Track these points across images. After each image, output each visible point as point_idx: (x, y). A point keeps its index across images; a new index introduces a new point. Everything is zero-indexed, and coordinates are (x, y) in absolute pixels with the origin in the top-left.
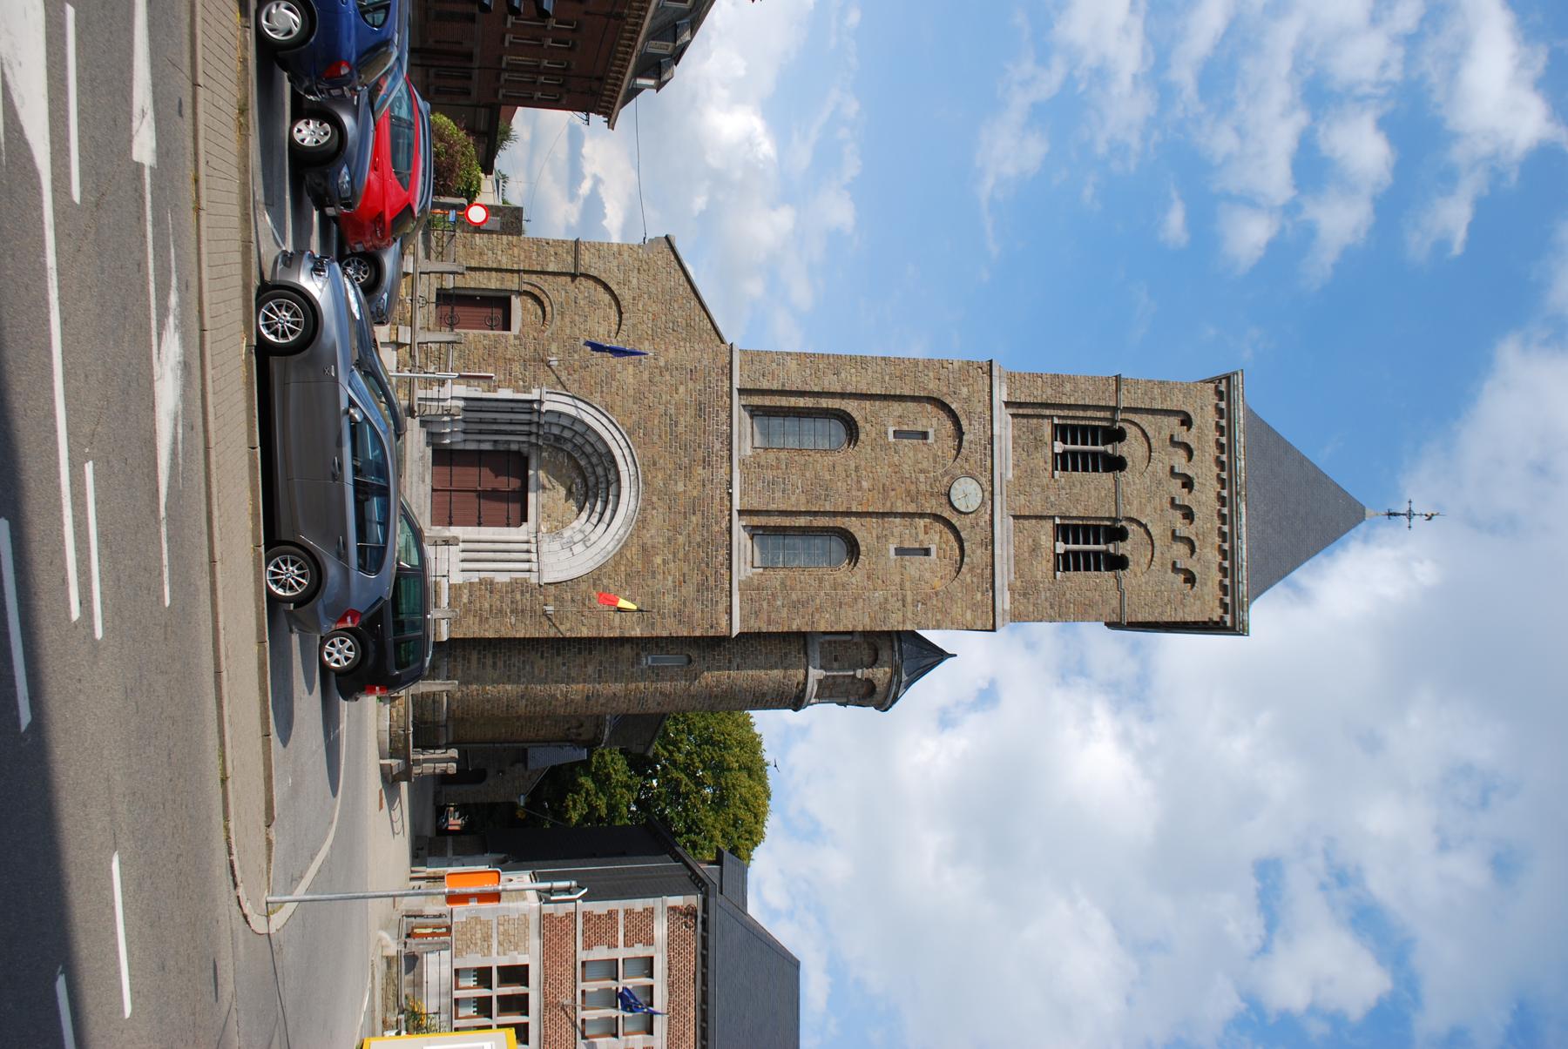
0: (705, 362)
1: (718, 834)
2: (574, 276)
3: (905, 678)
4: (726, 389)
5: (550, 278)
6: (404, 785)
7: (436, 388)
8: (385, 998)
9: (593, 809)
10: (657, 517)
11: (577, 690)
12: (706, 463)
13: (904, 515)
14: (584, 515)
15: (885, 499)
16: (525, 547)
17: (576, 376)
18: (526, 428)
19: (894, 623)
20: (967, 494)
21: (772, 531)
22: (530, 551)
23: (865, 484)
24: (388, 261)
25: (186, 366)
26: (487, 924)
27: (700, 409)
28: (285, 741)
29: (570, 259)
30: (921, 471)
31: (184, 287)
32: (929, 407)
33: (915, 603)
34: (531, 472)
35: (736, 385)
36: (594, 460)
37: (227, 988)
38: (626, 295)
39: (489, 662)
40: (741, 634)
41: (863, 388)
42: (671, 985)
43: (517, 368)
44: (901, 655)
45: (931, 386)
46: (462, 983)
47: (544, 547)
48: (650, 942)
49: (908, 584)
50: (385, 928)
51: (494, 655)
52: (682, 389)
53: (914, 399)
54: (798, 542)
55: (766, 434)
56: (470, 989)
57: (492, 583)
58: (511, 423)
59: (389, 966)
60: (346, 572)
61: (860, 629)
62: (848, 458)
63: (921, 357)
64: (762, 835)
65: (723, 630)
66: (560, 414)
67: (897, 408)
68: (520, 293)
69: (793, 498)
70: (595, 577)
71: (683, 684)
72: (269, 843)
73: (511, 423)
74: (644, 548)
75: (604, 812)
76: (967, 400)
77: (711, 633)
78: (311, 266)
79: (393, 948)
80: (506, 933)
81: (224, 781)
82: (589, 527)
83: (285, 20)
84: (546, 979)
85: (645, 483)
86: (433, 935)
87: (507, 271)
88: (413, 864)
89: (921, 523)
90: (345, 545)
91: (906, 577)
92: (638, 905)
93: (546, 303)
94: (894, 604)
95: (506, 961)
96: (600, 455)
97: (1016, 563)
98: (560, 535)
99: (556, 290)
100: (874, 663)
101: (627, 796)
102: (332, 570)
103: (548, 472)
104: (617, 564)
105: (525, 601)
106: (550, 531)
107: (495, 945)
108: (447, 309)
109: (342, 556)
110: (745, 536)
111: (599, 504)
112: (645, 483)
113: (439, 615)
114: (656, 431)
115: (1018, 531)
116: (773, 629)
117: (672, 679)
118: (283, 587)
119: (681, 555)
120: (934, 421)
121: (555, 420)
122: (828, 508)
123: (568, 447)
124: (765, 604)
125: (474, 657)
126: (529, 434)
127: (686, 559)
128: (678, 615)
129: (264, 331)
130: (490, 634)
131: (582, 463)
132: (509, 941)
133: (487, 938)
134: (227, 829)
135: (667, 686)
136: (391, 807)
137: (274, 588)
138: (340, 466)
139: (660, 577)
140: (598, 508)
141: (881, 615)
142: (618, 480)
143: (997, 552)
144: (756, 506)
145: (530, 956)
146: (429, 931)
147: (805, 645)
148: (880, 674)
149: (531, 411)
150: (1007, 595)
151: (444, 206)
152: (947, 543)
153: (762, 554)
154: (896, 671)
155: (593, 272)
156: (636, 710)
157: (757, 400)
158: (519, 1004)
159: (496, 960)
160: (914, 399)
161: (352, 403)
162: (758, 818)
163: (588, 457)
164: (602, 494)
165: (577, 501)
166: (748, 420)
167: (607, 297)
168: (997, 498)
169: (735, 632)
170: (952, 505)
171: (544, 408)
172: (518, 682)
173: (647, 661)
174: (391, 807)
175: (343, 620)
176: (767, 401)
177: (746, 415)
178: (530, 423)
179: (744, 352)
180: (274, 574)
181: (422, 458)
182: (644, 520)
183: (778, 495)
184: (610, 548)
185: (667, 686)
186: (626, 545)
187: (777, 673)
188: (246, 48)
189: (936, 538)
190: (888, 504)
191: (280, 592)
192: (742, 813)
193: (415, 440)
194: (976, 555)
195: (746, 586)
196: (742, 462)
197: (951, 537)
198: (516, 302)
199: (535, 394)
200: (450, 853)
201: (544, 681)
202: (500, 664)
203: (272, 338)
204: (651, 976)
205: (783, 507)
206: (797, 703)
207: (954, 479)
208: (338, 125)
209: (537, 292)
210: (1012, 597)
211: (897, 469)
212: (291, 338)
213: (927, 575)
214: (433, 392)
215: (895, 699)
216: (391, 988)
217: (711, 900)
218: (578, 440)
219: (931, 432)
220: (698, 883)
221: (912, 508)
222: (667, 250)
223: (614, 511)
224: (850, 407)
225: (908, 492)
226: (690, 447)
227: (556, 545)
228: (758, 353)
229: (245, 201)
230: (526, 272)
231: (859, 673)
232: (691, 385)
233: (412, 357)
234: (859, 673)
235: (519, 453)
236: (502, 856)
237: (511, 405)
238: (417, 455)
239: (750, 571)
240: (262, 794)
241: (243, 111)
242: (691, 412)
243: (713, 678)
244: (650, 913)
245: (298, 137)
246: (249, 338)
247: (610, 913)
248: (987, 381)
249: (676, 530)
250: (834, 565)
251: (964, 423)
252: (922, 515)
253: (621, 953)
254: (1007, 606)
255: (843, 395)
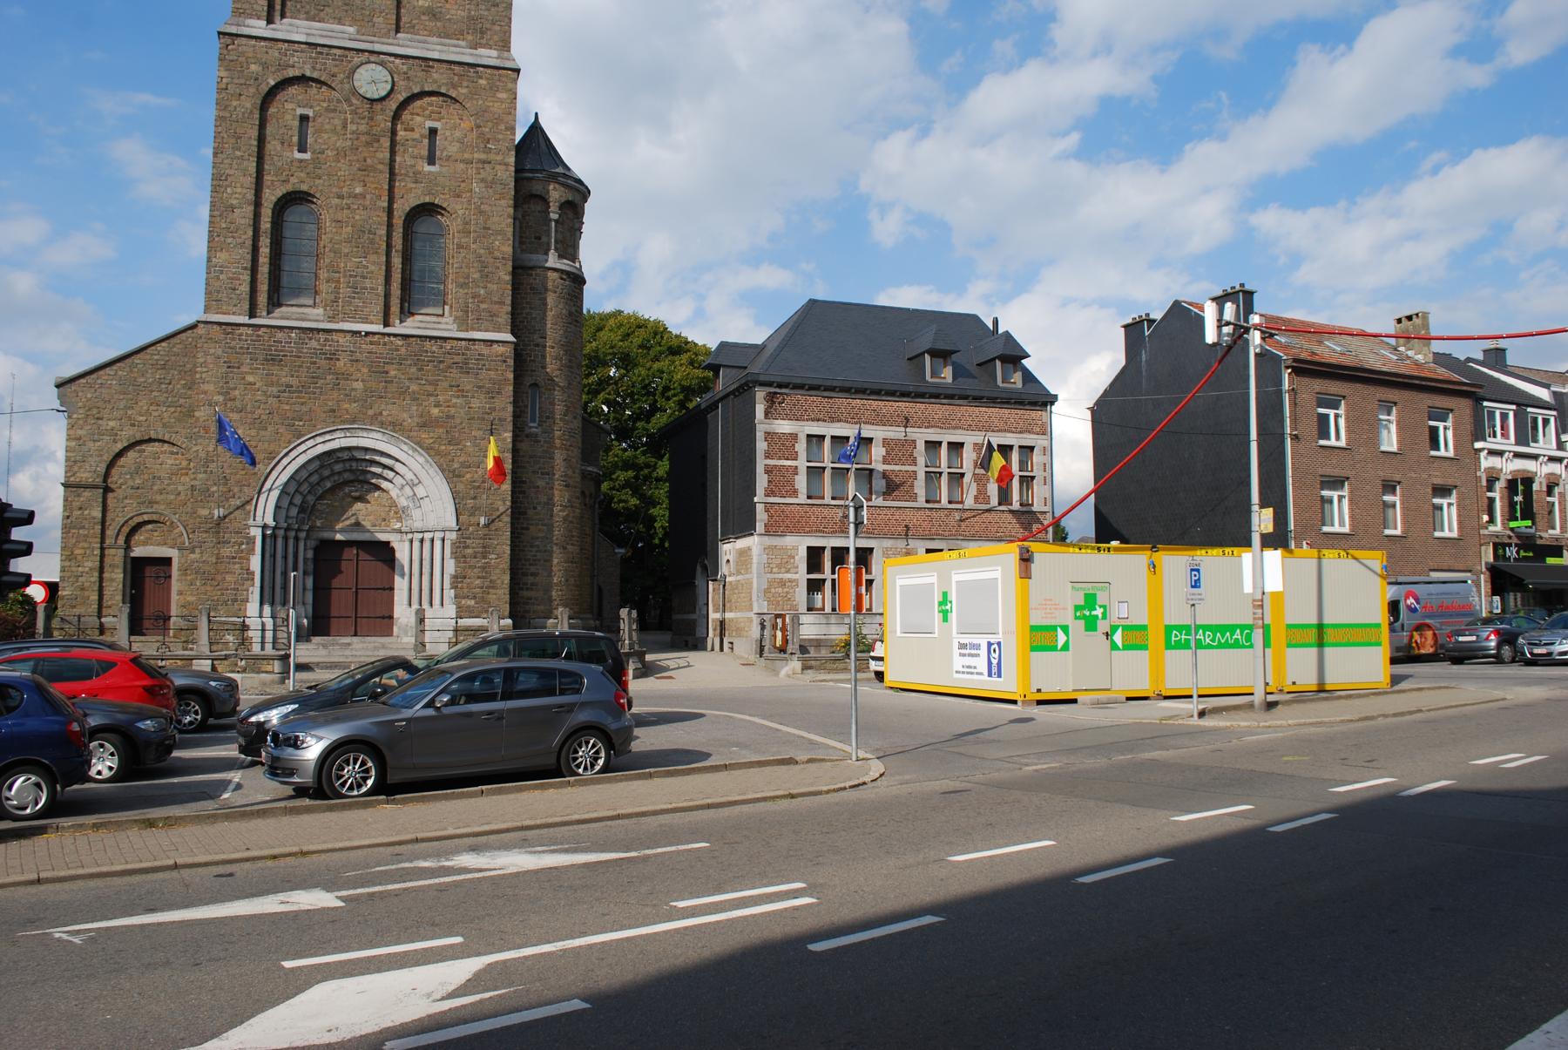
0: (220, 352)
1: (656, 366)
2: (107, 490)
3: (560, 170)
4: (250, 332)
5: (110, 516)
6: (649, 657)
7: (251, 634)
8: (837, 671)
9: (627, 484)
10: (389, 411)
11: (560, 496)
12: (332, 357)
13: (393, 152)
14: (385, 485)
15: (375, 170)
16: (416, 544)
17: (236, 490)
18: (291, 542)
19: (507, 174)
20: (372, 80)
21: (410, 292)
22: (422, 538)
23: (358, 190)
24: (179, 682)
25: (474, 849)
26: (771, 583)
27: (272, 360)
28: (707, 756)
29: (87, 493)
30: (345, 127)
31: (398, 857)
32: (272, 110)
33: (488, 151)
34: (339, 537)
35: (245, 319)
36: (326, 473)
37: (958, 785)
38: (127, 434)
39: (531, 579)
40: (513, 333)
41: (250, 181)
42: (833, 420)
43: (227, 551)
44: (537, 171)
45: (248, 105)
46: (819, 605)
47: (418, 525)
48: (794, 437)
49: (466, 156)
50: (776, 672)
51: (525, 574)
52: (250, 379)
53: (262, 126)
54: (418, 265)
55: (298, 291)
56: (824, 598)
57: (455, 577)
58: (285, 557)
59: (810, 668)
60: (583, 705)
61: (511, 211)
62: (328, 210)
63: (215, 113)
64: (657, 322)
65: (508, 351)
66: (277, 507)
67: (272, 146)
68: (128, 547)
69: (372, 268)
70: (452, 476)
71: (557, 393)
72: (810, 761)
73: (285, 557)
74: (423, 425)
75: (631, 473)
76: (265, 66)
77: (511, 362)
78: (290, 750)
79: (796, 664)
80: (779, 566)
81: (792, 796)
82: (398, 480)
83: (22, 789)
84: (819, 531)
85: (354, 421)
86: (784, 629)
87: (102, 561)
88: (705, 649)
89: (401, 134)
90: (561, 706)
91: (459, 156)
92: (761, 446)
93: (140, 519)
94: (487, 172)
95: (803, 567)
96: (322, 467)
97: (447, 36)
98: (404, 509)
99: (124, 510)
100: (544, 200)
101: (616, 450)
102: (582, 717)
103: (338, 521)
104: (438, 453)
105: (474, 545)
106: (400, 519)
107: (789, 576)
108: (147, 624)
109: (570, 708)
110: (410, 321)
111: (373, 469)
112: (354, 422)
113: (496, 627)
114: (297, 408)
115: (412, 29)
116: (508, 300)
117: (553, 404)
118: (596, 759)
119: (430, 388)
120: (289, 106)
121: (283, 512)
122: (384, 232)
123: (311, 499)
124: (483, 306)
125: (525, 593)
126: (297, 539)
127: (435, 384)
128: (492, 394)
129: (364, 789)
130: (507, 578)
131: (329, 485)
132: (786, 563)
133: (782, 583)
134: (828, 792)
135: (559, 408)
136: (667, 669)
137: (597, 768)
138: (490, 713)
139: (453, 410)
140: (378, 470)
141: (499, 188)
142: (349, 449)
143: (436, 55)
144: (379, 308)
145: (800, 545)
146: (779, 634)
147: (522, 268)
148: (556, 194)
149: (274, 536)
150: (482, 51)
151: (48, 631)
152: (424, 109)
153: (428, 306)
154: (554, 177)
155: (102, 469)
156: (579, 438)
157: (262, 299)
158: (839, 555)
159: (802, 575)
160: (262, 126)
161: (430, 704)
162: (641, 324)
163: (322, 479)
164: (363, 466)
165: (369, 491)
166: (284, 309)
167: (131, 454)
168: (377, 47)
169: (510, 338)
170: (382, 99)
171: (272, 523)
172: (551, 553)
173: (533, 427)
174: (667, 669)
175: (622, 706)
176: (263, 288)
177: (278, 312)
178: (286, 538)
179: (207, 310)
180: (585, 769)
181: (325, 646)
182: (393, 424)
183: (368, 283)
184: (421, 460)
185: (559, 408)
186: (417, 443)
187: (551, 299)
188: (81, 826)
189: (420, 120)
190: (381, 167)
191: (601, 762)
192: (637, 341)
193: (304, 652)
194: (437, 79)
195: (463, 324)
196: (332, 319)
197: (418, 103)
198: (138, 552)
199: (256, 533)
200: (693, 616)
201: (550, 528)
202: (533, 569)
203: (370, 782)
204: (823, 437)
205: (381, 280)
206: (578, 280)
207: (354, 92)
208: (95, 733)
209: (126, 529)
210: (484, 46)
211: (340, 154)
212: (370, 764)
213: (458, 134)
214: (254, 635)
215: (580, 182)
216: (829, 665)
217: (762, 378)
218: (305, 488)
219: (300, 111)
220: (744, 390)
221: (386, 143)
222: (74, 387)
223: (383, 454)
224: (270, 197)
225: (368, 144)
226: (315, 373)
227: (416, 514)
228: (208, 293)
229: (213, 818)
230: (103, 541)
231: (554, 216)
232: (245, 369)
233: (226, 658)
234: (554, 216)
235: (316, 550)
236: (699, 569)
237: (268, 557)
238: (323, 652)
239: (448, 319)
240: (776, 768)
241: (151, 824)
242: (275, 370)
243: (553, 363)
244: (769, 436)
245: (106, 774)
246: (380, 803)
247: (767, 472)
248: (244, 41)
249: (403, 392)
250: (442, 232)
251: (291, 73)
252: (394, 133)
253: (802, 463)
254: (494, 53)
255: (258, 204)
